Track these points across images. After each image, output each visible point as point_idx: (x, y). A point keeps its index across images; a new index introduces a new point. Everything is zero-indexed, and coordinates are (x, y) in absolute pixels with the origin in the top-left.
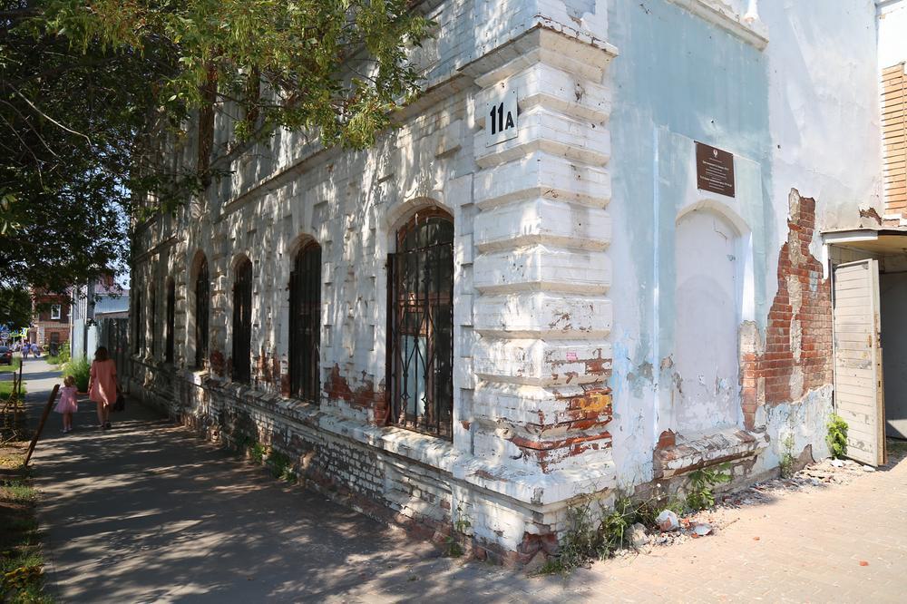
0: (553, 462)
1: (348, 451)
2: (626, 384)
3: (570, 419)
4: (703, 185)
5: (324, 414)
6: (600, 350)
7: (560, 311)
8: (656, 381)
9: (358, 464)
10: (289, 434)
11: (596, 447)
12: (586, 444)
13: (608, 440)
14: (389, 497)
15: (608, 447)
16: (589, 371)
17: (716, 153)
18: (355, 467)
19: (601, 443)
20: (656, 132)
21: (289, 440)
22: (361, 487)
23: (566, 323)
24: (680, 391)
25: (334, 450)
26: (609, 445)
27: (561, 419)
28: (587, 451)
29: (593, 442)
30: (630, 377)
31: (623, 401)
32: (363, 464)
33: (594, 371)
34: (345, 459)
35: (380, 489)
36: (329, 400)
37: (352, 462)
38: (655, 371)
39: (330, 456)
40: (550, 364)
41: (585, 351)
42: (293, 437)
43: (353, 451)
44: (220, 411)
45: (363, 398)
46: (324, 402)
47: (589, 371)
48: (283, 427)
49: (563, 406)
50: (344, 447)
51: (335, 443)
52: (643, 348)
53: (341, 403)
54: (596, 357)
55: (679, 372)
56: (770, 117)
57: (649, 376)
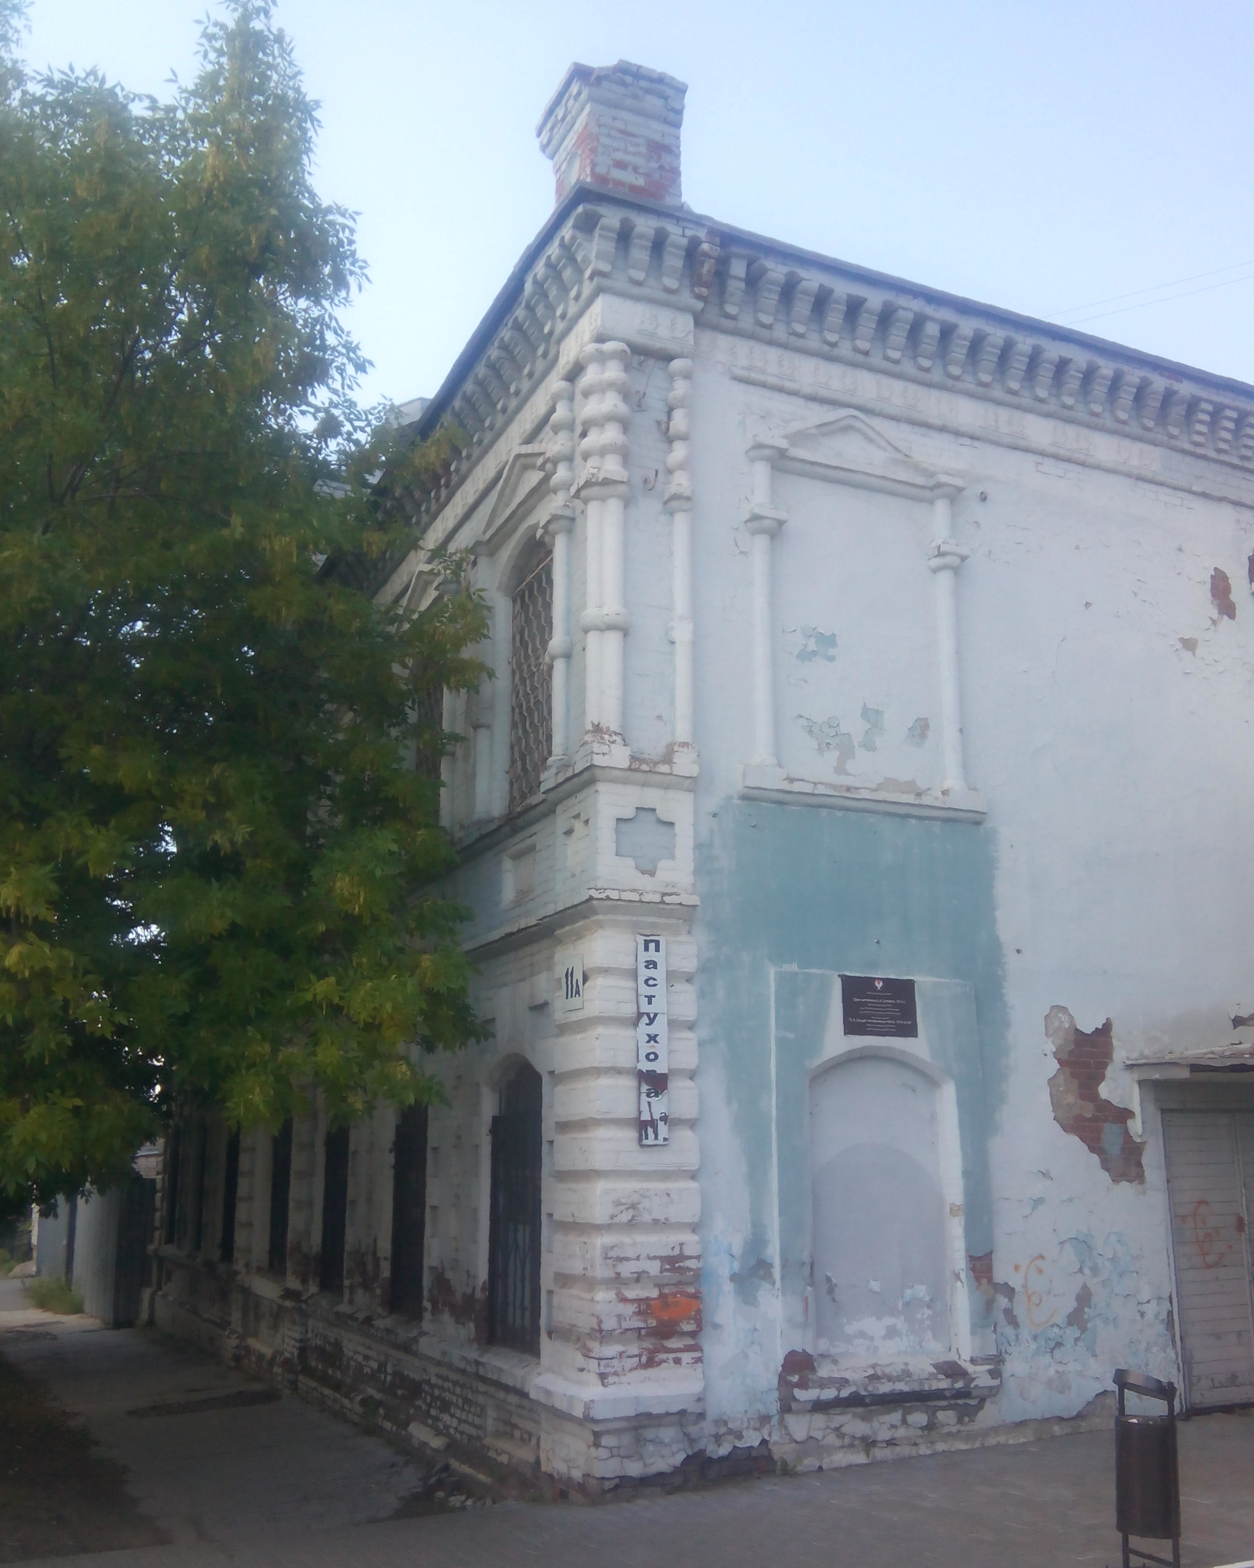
0: (616, 1374)
1: (450, 1385)
2: (728, 1287)
3: (642, 1325)
4: (851, 1028)
5: (427, 1333)
6: (681, 1245)
7: (624, 1201)
8: (778, 1284)
9: (460, 1402)
10: (389, 1370)
11: (677, 1361)
12: (663, 1356)
13: (697, 1354)
14: (488, 1441)
15: (696, 1362)
16: (666, 1270)
17: (879, 985)
18: (457, 1406)
19: (686, 1357)
20: (772, 972)
21: (389, 1378)
22: (462, 1433)
23: (631, 1212)
24: (834, 1300)
25: (436, 1386)
26: (699, 1360)
27: (625, 1325)
28: (664, 1365)
29: (674, 1355)
30: (734, 1278)
31: (725, 1307)
32: (467, 1401)
33: (671, 1270)
34: (447, 1396)
35: (480, 1433)
36: (433, 1313)
37: (454, 1399)
38: (777, 1273)
39: (432, 1395)
40: (610, 1262)
41: (662, 1243)
42: (395, 1374)
43: (456, 1383)
44: (301, 1341)
45: (462, 1310)
46: (427, 1316)
47: (666, 1270)
48: (382, 1358)
49: (630, 1309)
50: (446, 1379)
51: (438, 1376)
52: (757, 1242)
53: (446, 1317)
54: (677, 1252)
55: (829, 1274)
56: (997, 913)
57: (768, 1277)
